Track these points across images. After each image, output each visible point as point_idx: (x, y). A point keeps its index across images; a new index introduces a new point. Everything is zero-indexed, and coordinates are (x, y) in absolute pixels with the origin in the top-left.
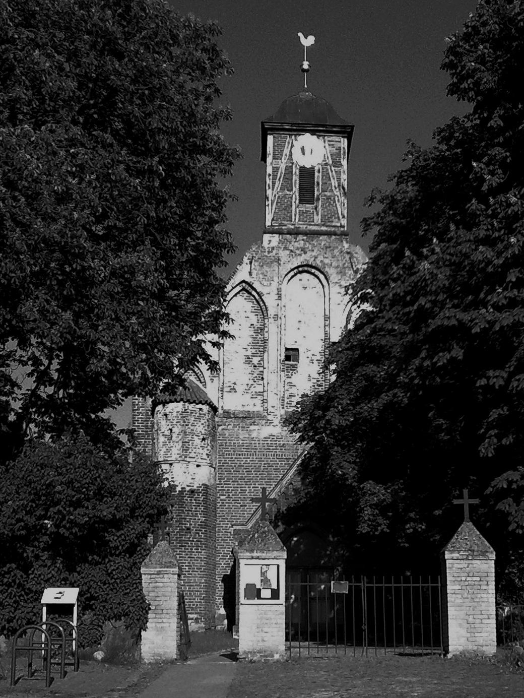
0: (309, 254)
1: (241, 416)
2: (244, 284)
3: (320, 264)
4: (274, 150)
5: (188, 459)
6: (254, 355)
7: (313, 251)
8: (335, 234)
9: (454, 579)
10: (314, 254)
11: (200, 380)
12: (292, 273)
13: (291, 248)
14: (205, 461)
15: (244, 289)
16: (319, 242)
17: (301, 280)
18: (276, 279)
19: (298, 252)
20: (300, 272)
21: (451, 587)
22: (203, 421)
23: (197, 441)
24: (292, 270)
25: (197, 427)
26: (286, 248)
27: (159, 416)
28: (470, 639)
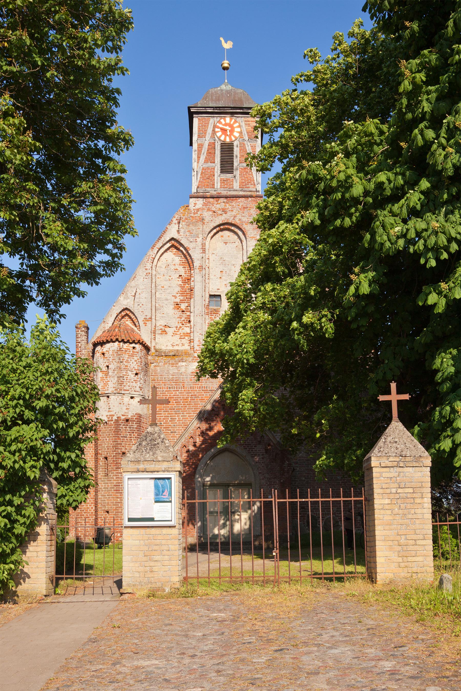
0: (229, 214)
1: (171, 354)
2: (173, 242)
3: (238, 222)
4: (199, 129)
5: (123, 392)
6: (182, 301)
7: (232, 211)
8: (251, 196)
9: (381, 491)
10: (234, 213)
11: (135, 325)
12: (215, 231)
13: (214, 209)
14: (138, 393)
15: (173, 246)
16: (237, 204)
17: (222, 236)
18: (200, 236)
19: (220, 212)
20: (222, 230)
21: (379, 501)
22: (136, 358)
23: (131, 375)
24: (215, 228)
25: (131, 363)
26: (209, 210)
27: (97, 355)
28: (402, 565)
